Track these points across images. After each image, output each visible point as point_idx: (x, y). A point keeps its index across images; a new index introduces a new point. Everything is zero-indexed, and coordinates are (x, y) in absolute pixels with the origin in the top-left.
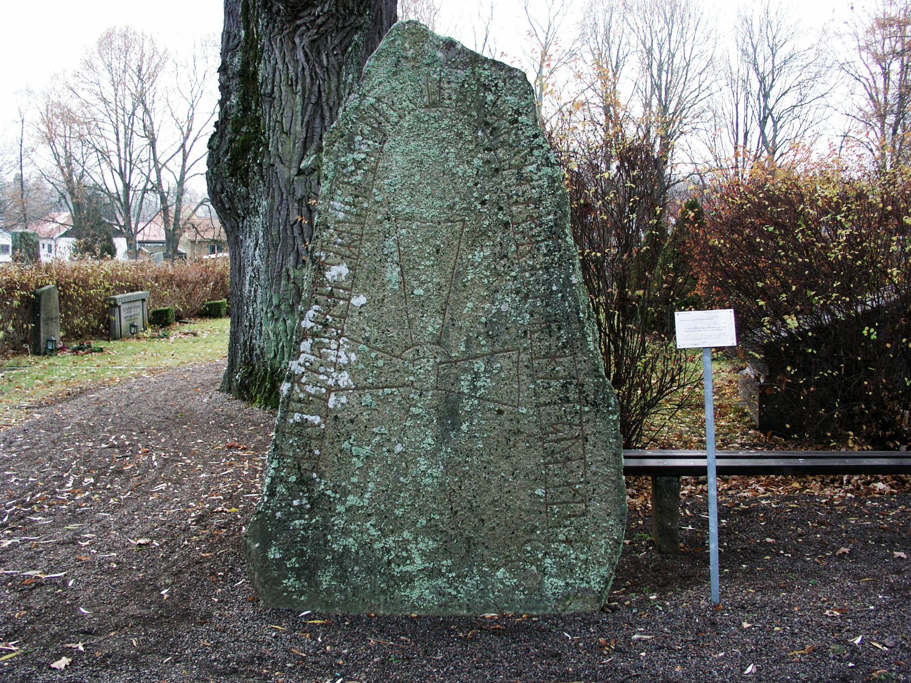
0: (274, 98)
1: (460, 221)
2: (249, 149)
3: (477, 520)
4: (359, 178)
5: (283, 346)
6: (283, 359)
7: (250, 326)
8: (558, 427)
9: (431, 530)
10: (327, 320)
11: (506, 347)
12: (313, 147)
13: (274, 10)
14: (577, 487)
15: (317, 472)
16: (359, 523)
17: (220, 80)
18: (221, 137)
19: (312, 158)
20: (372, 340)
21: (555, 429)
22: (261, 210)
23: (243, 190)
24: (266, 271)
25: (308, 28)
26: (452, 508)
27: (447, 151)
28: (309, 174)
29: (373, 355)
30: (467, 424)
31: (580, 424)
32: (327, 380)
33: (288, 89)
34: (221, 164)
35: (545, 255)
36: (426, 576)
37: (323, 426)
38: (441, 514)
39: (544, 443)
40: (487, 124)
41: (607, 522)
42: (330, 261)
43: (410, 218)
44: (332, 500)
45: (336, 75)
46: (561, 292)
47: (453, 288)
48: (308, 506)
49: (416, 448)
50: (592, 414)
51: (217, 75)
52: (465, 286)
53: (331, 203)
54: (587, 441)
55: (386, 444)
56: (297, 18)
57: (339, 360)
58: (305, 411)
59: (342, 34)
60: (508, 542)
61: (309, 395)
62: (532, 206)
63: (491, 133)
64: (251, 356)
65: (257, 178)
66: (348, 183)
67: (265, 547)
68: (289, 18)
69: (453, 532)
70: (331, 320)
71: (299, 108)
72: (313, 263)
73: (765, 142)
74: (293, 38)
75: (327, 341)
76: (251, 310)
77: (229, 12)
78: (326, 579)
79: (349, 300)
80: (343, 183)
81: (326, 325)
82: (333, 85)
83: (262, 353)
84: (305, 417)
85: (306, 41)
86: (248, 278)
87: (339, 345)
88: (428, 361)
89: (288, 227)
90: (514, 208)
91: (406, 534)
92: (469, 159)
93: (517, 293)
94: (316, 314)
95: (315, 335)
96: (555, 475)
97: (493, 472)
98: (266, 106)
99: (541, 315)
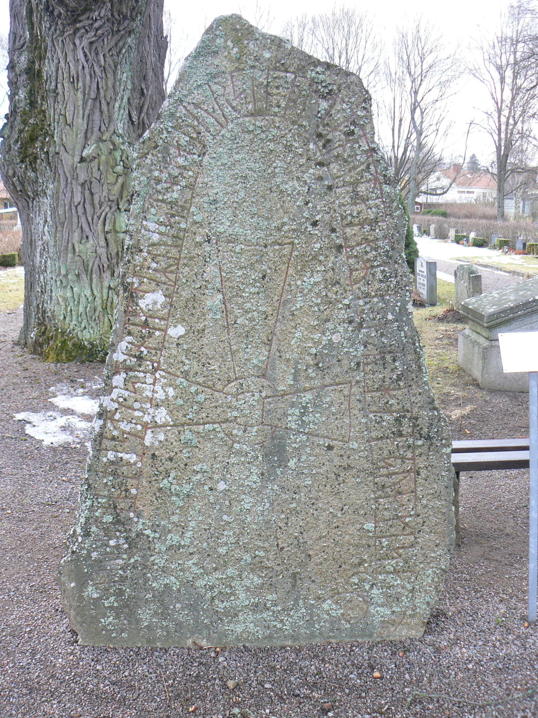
0: (58, 94)
1: (289, 243)
2: (37, 139)
3: (303, 555)
4: (175, 195)
5: (71, 310)
6: (71, 321)
7: (42, 291)
8: (389, 461)
9: (257, 566)
10: (142, 352)
11: (337, 380)
12: (94, 138)
13: (56, 13)
14: (407, 520)
15: (135, 512)
16: (180, 562)
17: (8, 77)
18: (12, 127)
19: (93, 148)
20: (191, 374)
21: (386, 463)
22: (49, 192)
23: (32, 175)
24: (55, 246)
25: (86, 30)
26: (278, 545)
27: (275, 165)
28: (91, 161)
29: (193, 389)
30: (295, 460)
31: (413, 459)
32: (142, 417)
33: (70, 85)
34: (12, 152)
35: (381, 281)
36: (251, 610)
37: (139, 465)
38: (266, 551)
39: (374, 478)
40: (320, 135)
41: (435, 552)
42: (144, 287)
43: (233, 240)
44: (150, 539)
45: (112, 73)
46: (397, 321)
47: (280, 317)
48: (126, 546)
49: (240, 486)
50: (426, 448)
51: (6, 72)
52: (293, 315)
53: (144, 223)
54: (419, 474)
55: (208, 482)
56: (76, 21)
57: (156, 395)
58: (119, 449)
59: (116, 38)
60: (336, 575)
61: (124, 432)
62: (368, 228)
63: (324, 146)
64: (44, 318)
65: (44, 164)
66: (163, 201)
67: (82, 585)
68: (69, 22)
69: (278, 568)
70: (145, 352)
71: (80, 103)
72: (125, 290)
73: (415, 127)
74: (74, 40)
75: (142, 375)
76: (42, 278)
77: (14, 15)
78: (145, 615)
79: (166, 331)
80: (158, 200)
81: (140, 358)
82: (110, 83)
83: (53, 316)
84: (120, 455)
85: (85, 43)
86: (38, 250)
87: (155, 379)
88: (253, 395)
89: (73, 208)
90: (348, 230)
91: (230, 571)
92: (300, 174)
93: (350, 322)
94: (129, 346)
95: (128, 369)
96: (386, 509)
97: (321, 509)
98: (51, 101)
99: (375, 345)
